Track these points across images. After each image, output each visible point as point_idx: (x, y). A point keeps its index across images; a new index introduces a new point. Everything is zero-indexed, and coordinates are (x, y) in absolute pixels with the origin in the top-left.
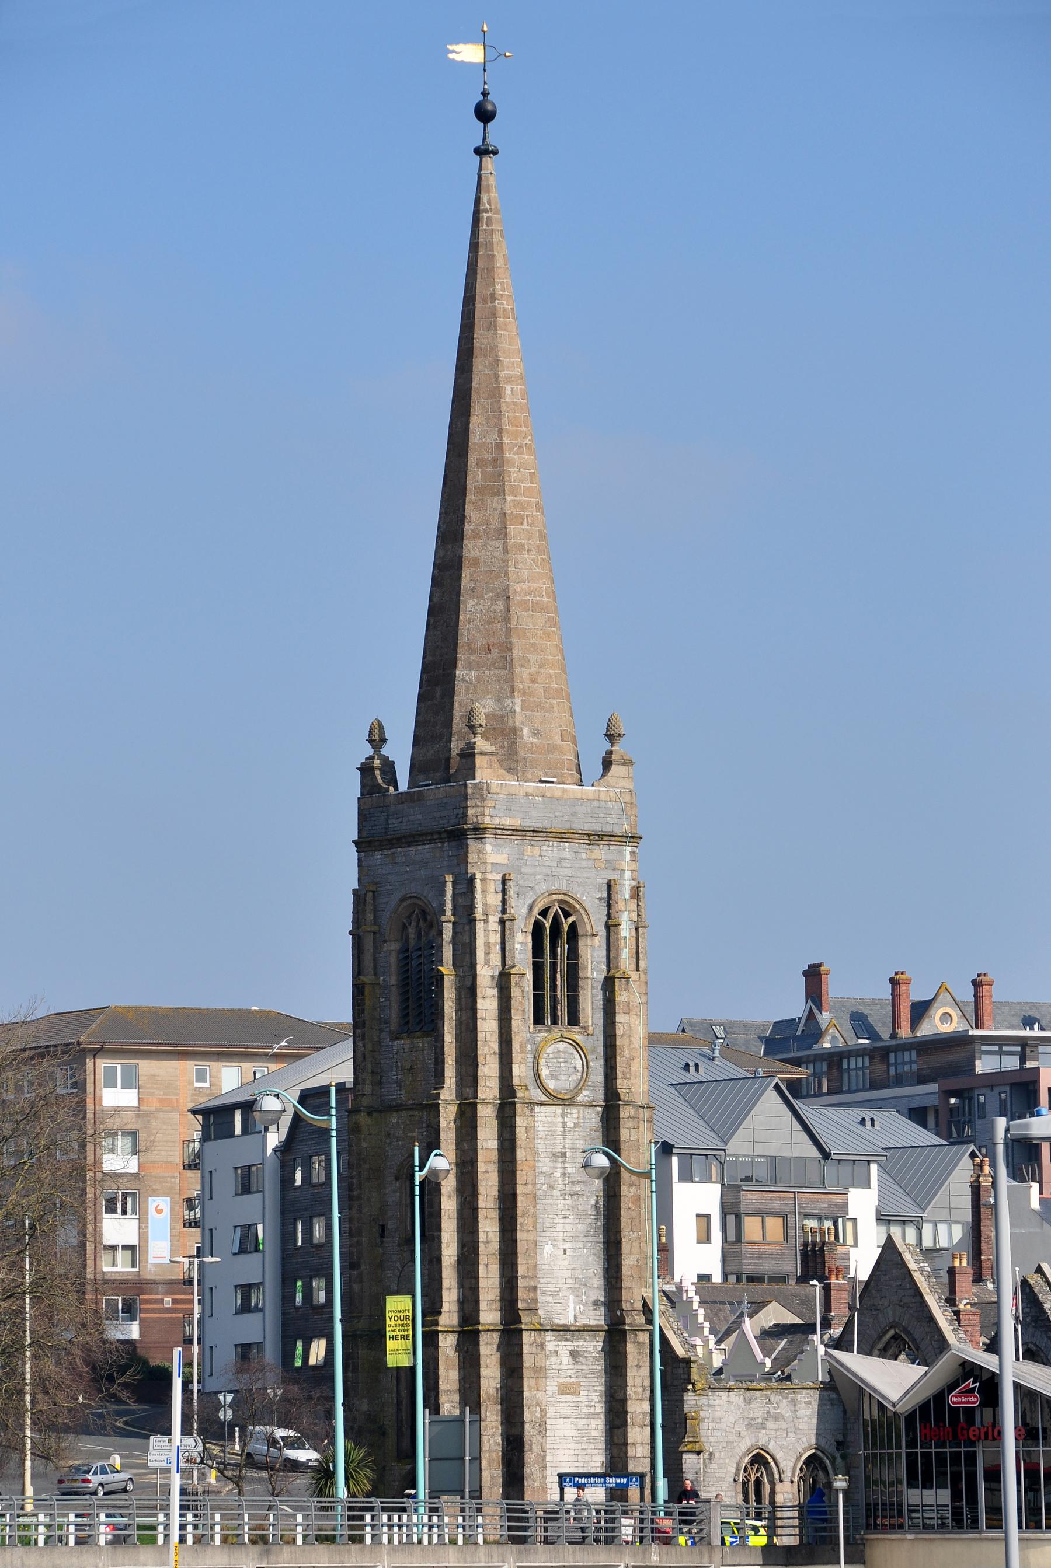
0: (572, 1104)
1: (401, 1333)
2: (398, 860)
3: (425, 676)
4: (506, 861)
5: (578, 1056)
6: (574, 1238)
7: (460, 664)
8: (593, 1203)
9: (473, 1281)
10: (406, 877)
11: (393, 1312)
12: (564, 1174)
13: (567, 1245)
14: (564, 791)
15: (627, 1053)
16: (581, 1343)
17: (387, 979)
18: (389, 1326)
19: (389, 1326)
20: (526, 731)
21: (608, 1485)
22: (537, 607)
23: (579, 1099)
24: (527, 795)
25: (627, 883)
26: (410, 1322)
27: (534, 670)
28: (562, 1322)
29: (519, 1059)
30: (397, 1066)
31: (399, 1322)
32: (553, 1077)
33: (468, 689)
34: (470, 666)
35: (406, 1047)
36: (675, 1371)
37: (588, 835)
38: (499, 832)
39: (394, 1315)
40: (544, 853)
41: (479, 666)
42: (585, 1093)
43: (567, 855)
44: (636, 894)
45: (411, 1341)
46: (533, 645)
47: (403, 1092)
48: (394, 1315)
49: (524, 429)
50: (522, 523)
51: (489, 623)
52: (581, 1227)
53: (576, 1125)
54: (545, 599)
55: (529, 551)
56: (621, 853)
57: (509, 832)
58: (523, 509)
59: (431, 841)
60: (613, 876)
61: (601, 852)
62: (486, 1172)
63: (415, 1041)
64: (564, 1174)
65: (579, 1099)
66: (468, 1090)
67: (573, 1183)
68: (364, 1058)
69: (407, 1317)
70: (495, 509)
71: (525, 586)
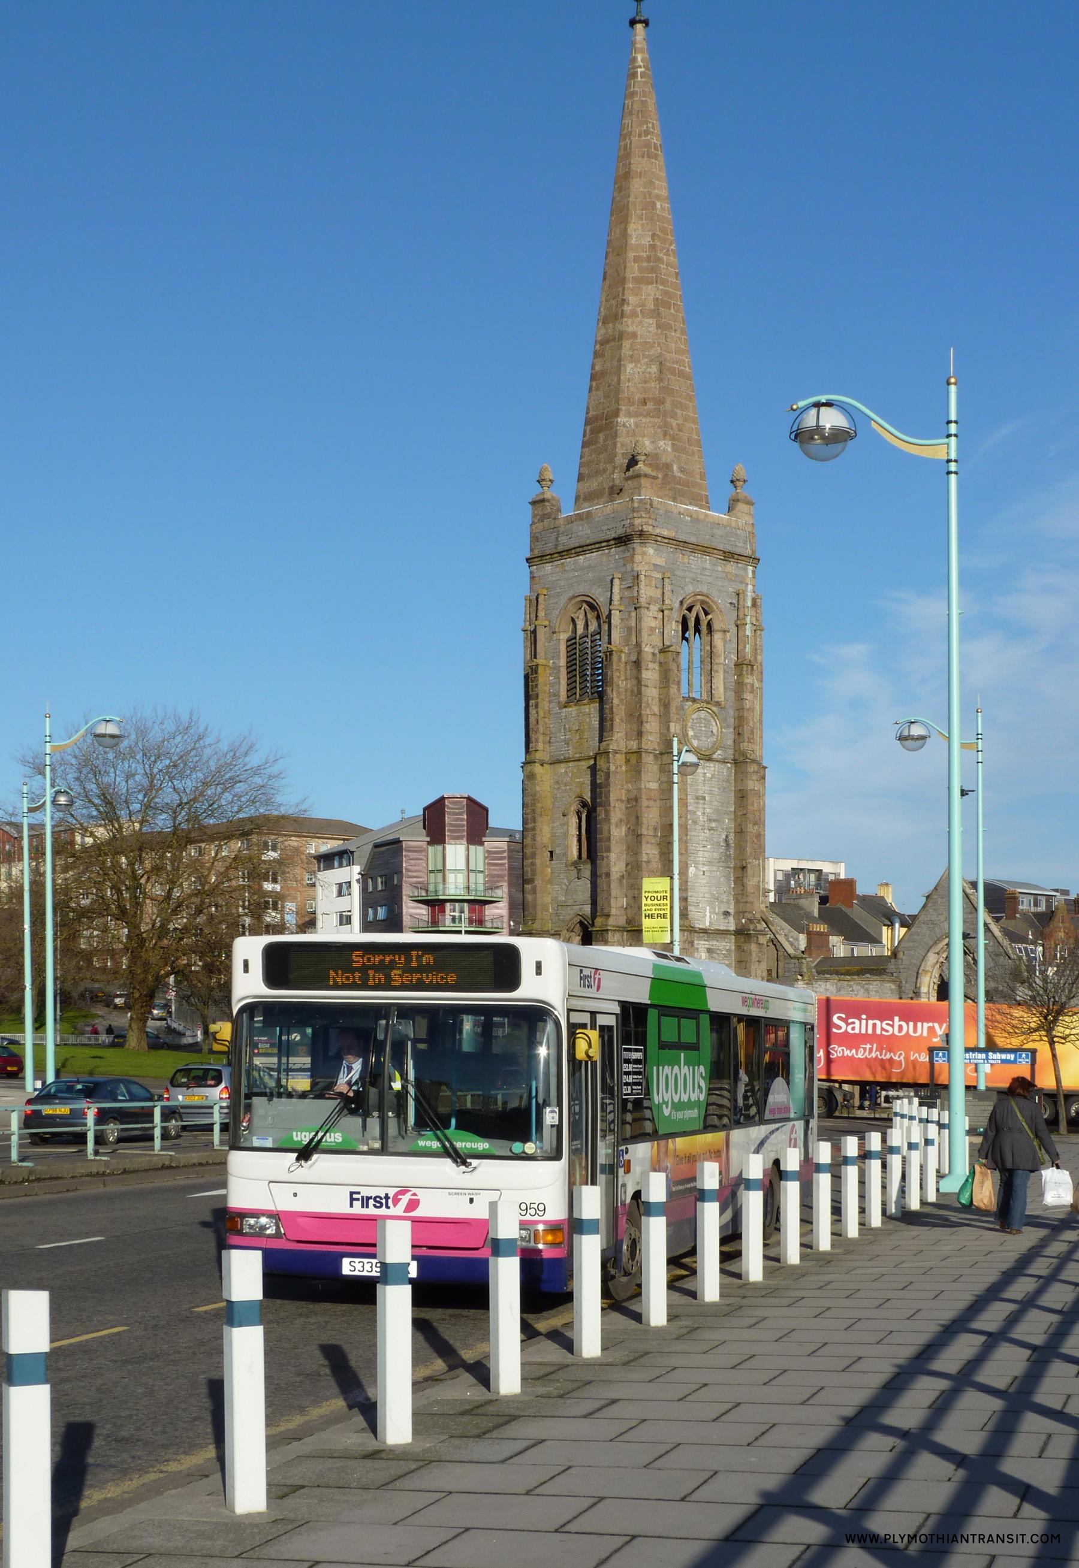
0: (710, 760)
1: (657, 912)
2: (567, 568)
3: (588, 428)
4: (664, 564)
5: (714, 724)
6: (710, 863)
7: (622, 413)
8: (724, 837)
9: (636, 892)
10: (574, 580)
11: (649, 892)
12: (704, 813)
13: (705, 868)
14: (706, 515)
15: (751, 724)
16: (715, 943)
17: (557, 661)
18: (645, 905)
19: (645, 905)
20: (675, 467)
21: (992, 1062)
22: (682, 375)
23: (715, 756)
24: (680, 513)
25: (749, 594)
26: (668, 902)
27: (680, 422)
28: (701, 927)
29: (675, 719)
30: (565, 728)
31: (656, 902)
32: (696, 737)
33: (628, 433)
34: (629, 415)
35: (574, 713)
36: (787, 966)
37: (725, 552)
38: (659, 539)
39: (650, 895)
40: (691, 562)
41: (637, 415)
42: (719, 752)
43: (708, 566)
44: (754, 604)
45: (669, 919)
46: (680, 403)
47: (570, 748)
48: (650, 895)
49: (670, 237)
50: (670, 309)
51: (645, 382)
52: (716, 855)
53: (713, 776)
54: (687, 369)
55: (675, 330)
56: (746, 570)
57: (666, 541)
58: (670, 298)
59: (598, 549)
60: (741, 587)
61: (731, 567)
62: (648, 807)
63: (582, 707)
64: (704, 813)
65: (715, 756)
66: (632, 742)
67: (710, 820)
68: (538, 722)
69: (665, 898)
70: (649, 295)
71: (674, 356)
